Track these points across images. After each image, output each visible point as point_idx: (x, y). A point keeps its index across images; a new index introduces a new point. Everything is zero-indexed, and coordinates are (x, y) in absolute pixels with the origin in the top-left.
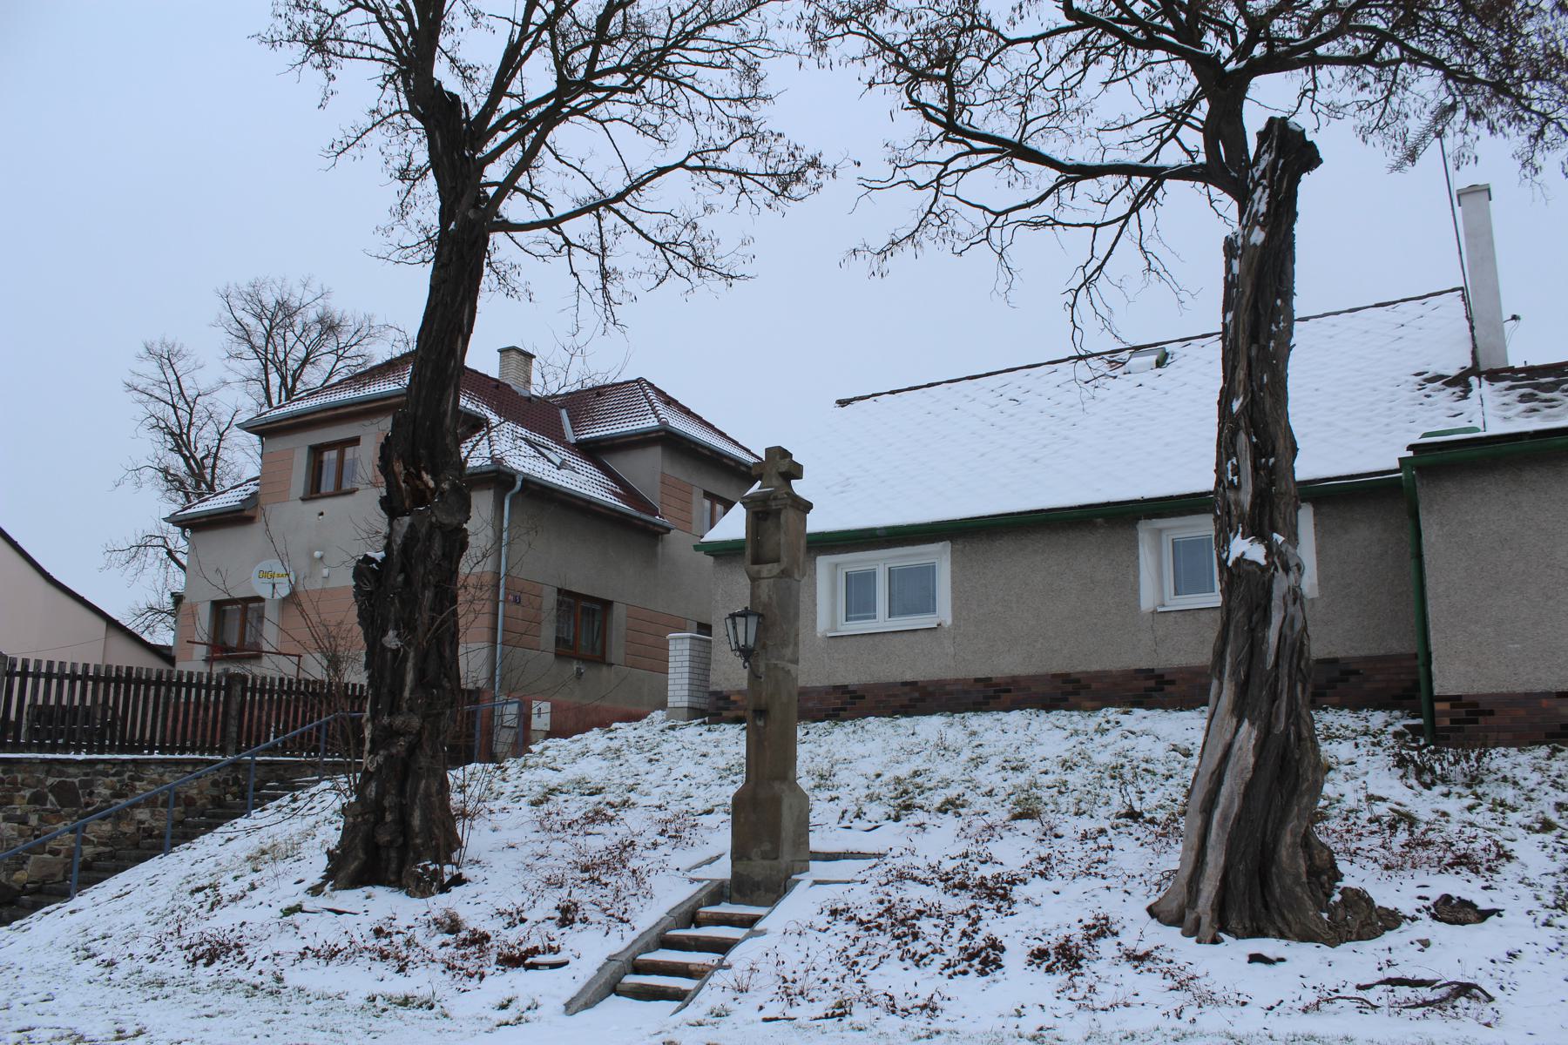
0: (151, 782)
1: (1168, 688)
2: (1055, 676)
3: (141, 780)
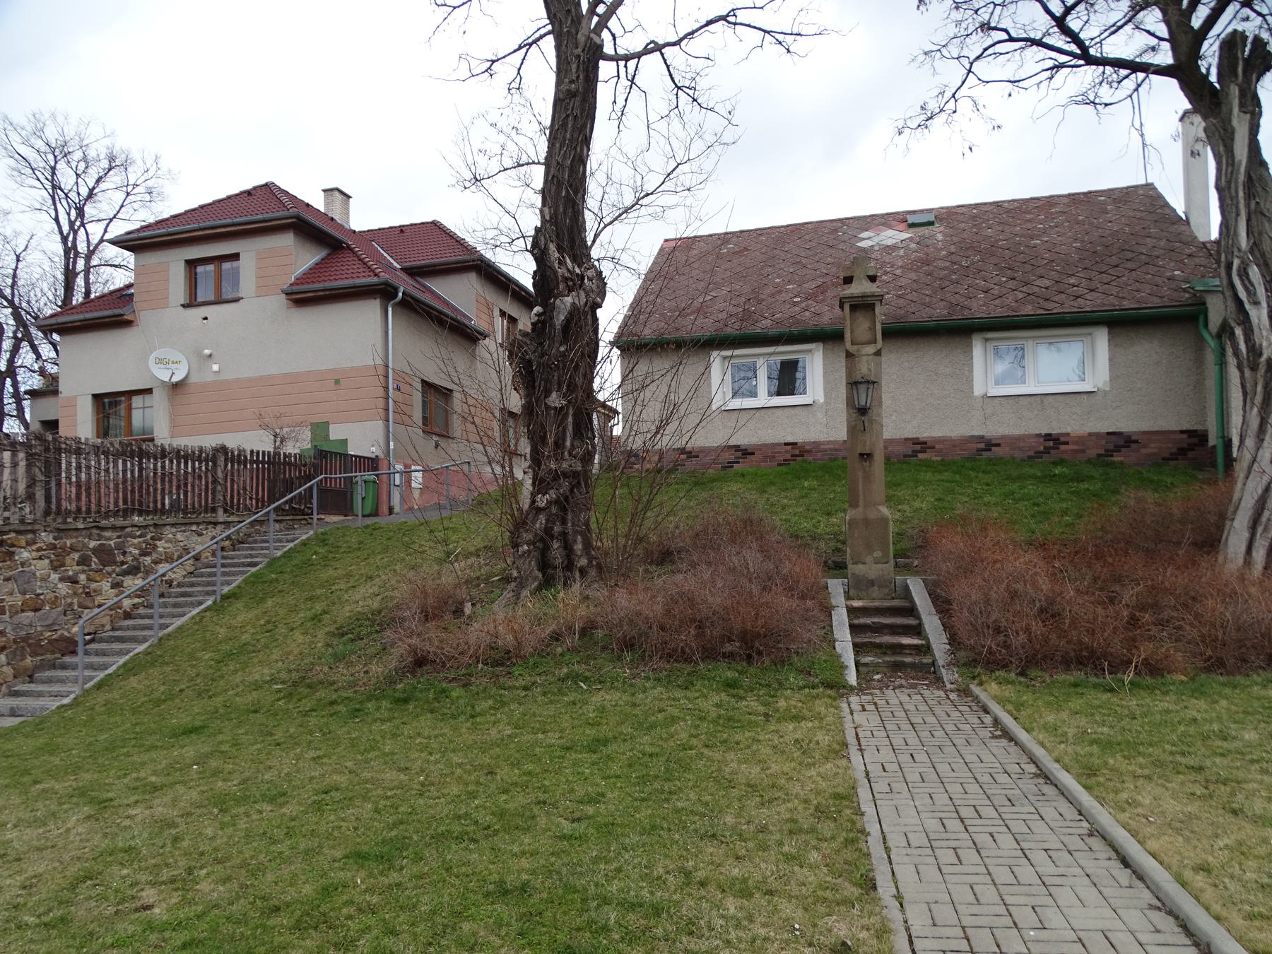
0: (169, 541)
1: (1063, 447)
2: (906, 439)
3: (160, 539)
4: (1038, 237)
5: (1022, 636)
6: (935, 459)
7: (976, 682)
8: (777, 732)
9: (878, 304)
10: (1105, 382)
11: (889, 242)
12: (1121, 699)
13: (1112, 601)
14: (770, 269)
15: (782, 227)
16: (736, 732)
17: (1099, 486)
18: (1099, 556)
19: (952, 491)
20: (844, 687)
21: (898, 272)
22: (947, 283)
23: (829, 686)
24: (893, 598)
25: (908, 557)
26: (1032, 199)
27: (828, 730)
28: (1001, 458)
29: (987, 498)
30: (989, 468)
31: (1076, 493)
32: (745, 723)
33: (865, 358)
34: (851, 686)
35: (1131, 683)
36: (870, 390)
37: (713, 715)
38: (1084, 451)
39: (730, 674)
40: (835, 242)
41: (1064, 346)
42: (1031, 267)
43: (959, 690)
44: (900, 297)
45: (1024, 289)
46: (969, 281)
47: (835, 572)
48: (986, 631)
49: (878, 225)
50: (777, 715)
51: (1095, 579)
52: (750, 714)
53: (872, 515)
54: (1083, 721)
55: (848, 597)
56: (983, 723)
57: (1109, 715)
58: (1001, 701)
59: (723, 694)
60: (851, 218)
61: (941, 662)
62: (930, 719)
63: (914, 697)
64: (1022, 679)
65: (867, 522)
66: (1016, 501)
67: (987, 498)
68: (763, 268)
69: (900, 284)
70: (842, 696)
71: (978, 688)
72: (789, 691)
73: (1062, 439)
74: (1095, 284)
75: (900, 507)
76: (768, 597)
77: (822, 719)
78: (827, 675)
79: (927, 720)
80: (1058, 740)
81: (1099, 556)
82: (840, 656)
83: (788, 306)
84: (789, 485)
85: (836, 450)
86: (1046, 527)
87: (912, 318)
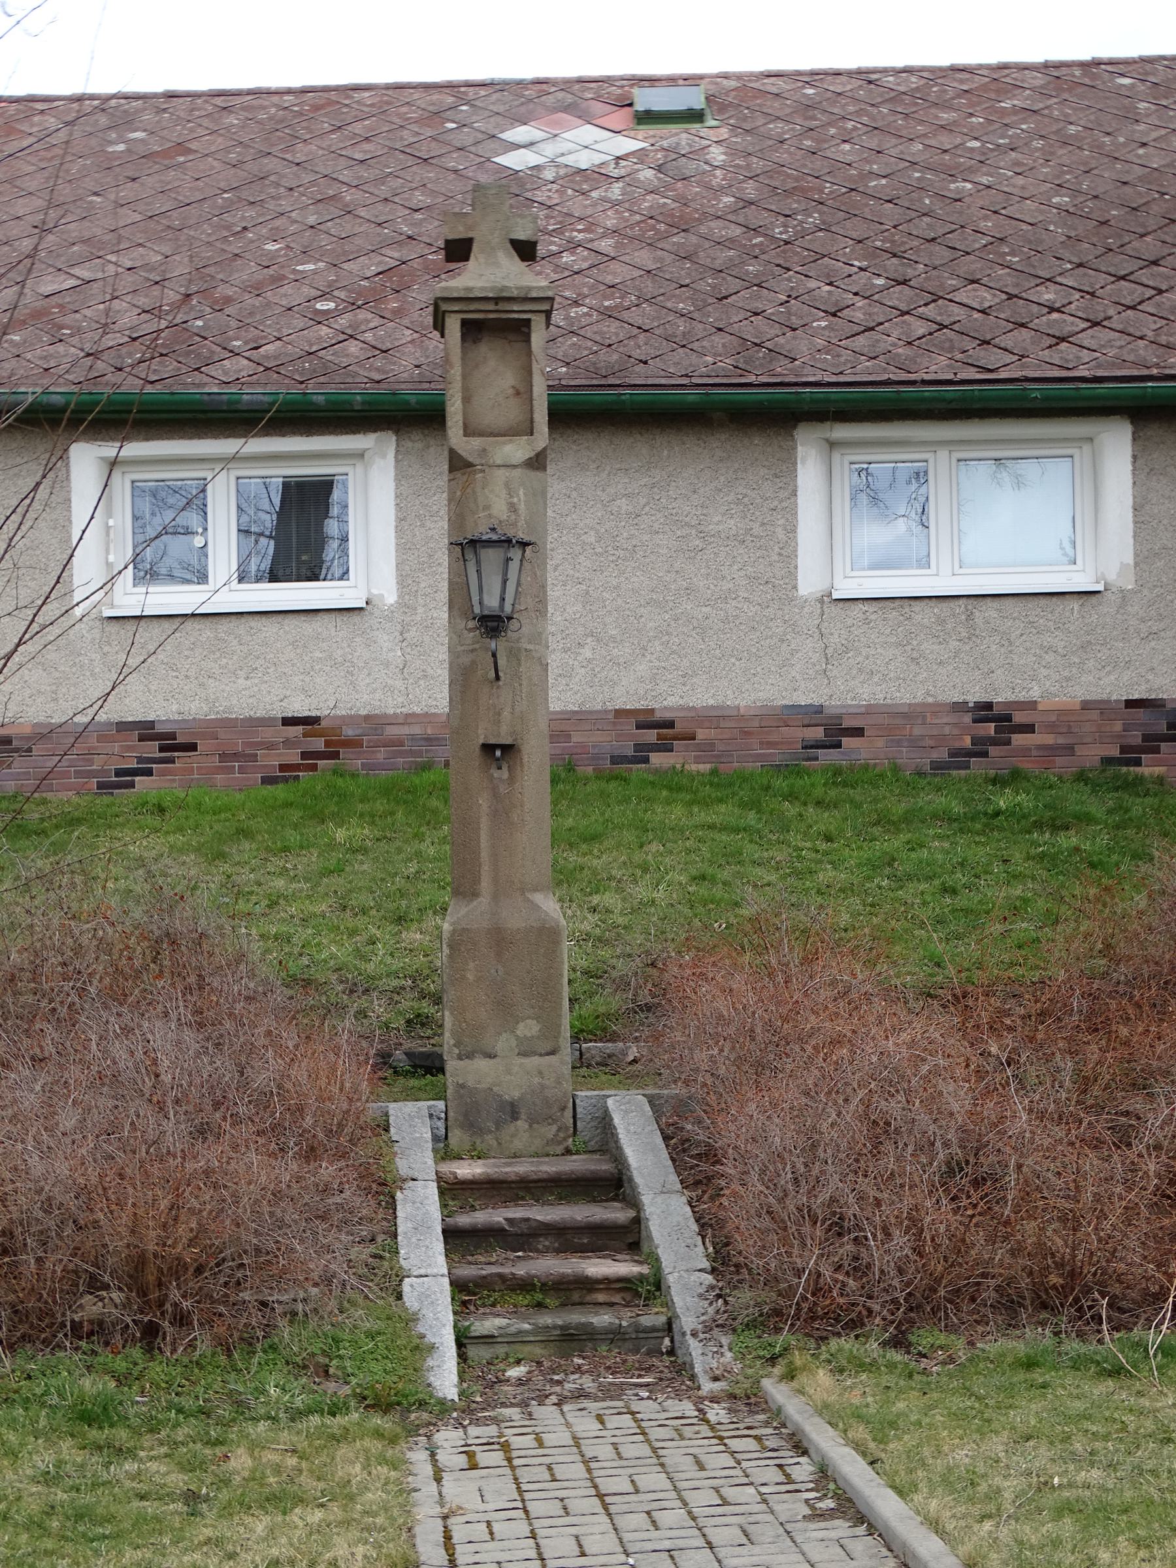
1: (1018, 739)
2: (619, 713)
4: (964, 174)
5: (900, 1239)
6: (694, 767)
7: (777, 1370)
8: (218, 1542)
9: (538, 322)
10: (1123, 566)
11: (584, 160)
12: (1140, 1394)
13: (1124, 1140)
14: (250, 213)
15: (289, 91)
16: (97, 1553)
17: (1104, 839)
18: (1096, 1024)
19: (734, 856)
20: (422, 1404)
21: (606, 245)
22: (735, 284)
23: (379, 1403)
24: (568, 1152)
25: (614, 1038)
26: (955, 69)
27: (367, 1529)
28: (866, 767)
29: (827, 875)
30: (833, 793)
31: (1049, 860)
32: (127, 1525)
33: (501, 474)
34: (442, 1402)
35: (1163, 1349)
36: (514, 566)
37: (33, 1506)
38: (1069, 750)
39: (90, 1385)
40: (436, 149)
41: (1029, 469)
42: (948, 254)
43: (733, 1397)
44: (608, 314)
45: (930, 311)
46: (791, 281)
47: (413, 1082)
48: (807, 1229)
49: (556, 110)
50: (224, 1495)
51: (1084, 1083)
52: (142, 1498)
53: (515, 919)
54: (1041, 1456)
55: (444, 1151)
56: (789, 1480)
57: (1106, 1438)
58: (831, 1415)
59: (66, 1445)
60: (483, 85)
61: (688, 1322)
62: (653, 1480)
63: (613, 1422)
64: (896, 1356)
65: (500, 939)
66: (900, 881)
67: (827, 875)
68: (227, 209)
69: (610, 279)
70: (412, 1431)
71: (783, 1387)
72: (262, 1426)
73: (1019, 718)
74: (1099, 309)
75: (596, 899)
76: (210, 1155)
77: (351, 1498)
78: (376, 1374)
79: (643, 1482)
80: (976, 1510)
81: (1096, 1024)
82: (411, 1319)
83: (300, 323)
84: (293, 837)
85: (429, 740)
86: (969, 949)
87: (640, 374)
